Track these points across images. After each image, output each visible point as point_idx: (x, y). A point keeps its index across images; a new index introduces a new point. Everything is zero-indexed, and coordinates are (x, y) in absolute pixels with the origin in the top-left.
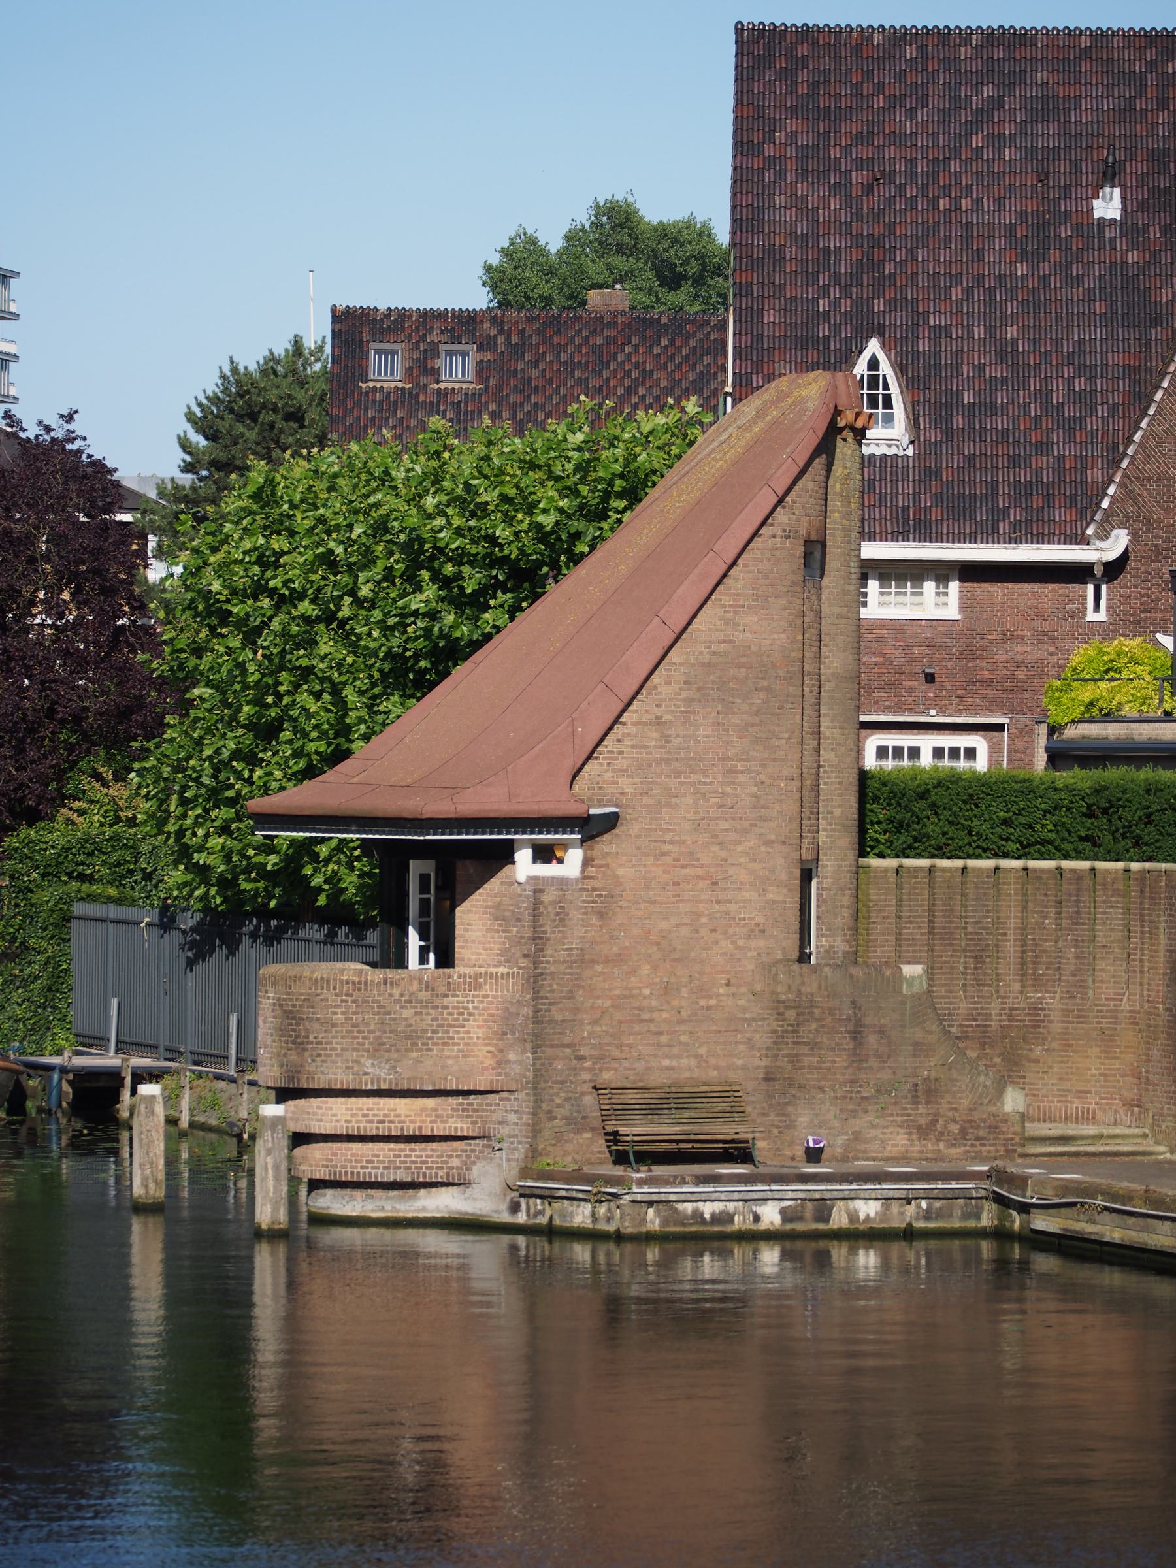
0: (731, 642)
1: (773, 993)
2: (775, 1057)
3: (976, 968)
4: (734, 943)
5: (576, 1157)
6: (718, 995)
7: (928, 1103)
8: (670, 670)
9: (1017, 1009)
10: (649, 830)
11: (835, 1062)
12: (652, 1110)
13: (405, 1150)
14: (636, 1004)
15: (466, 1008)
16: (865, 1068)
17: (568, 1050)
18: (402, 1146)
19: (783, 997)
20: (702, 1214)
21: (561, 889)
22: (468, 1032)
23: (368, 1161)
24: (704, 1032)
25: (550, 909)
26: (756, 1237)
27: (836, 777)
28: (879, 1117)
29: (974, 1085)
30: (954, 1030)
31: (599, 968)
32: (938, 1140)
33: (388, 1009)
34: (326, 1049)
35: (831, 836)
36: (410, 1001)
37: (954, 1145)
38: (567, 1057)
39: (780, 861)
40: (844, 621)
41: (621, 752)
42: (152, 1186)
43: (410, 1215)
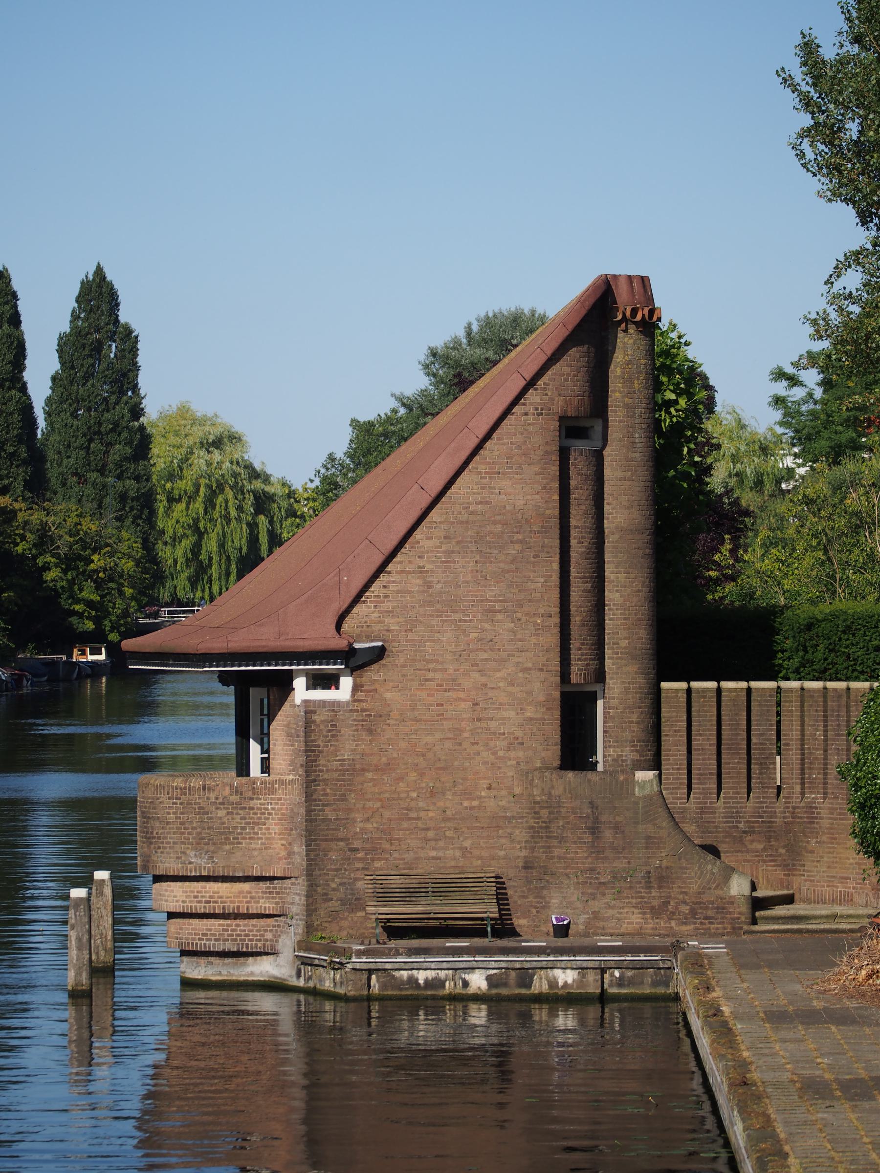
0: (487, 503)
1: (530, 795)
2: (533, 849)
3: (760, 773)
4: (495, 753)
5: (351, 931)
6: (480, 797)
7: (660, 887)
8: (431, 528)
9: (798, 807)
10: (415, 660)
11: (577, 853)
12: (410, 894)
13: (231, 925)
14: (404, 804)
15: (266, 809)
16: (602, 858)
17: (342, 844)
18: (229, 922)
19: (538, 799)
20: (417, 980)
21: (333, 710)
22: (268, 829)
23: (203, 935)
24: (468, 828)
25: (322, 727)
26: (464, 999)
27: (621, 614)
28: (614, 900)
29: (702, 872)
30: (741, 825)
31: (369, 775)
32: (670, 919)
33: (206, 810)
34: (163, 843)
35: (617, 664)
36: (223, 804)
37: (685, 924)
38: (341, 849)
39: (537, 686)
40: (628, 483)
41: (386, 596)
42: (102, 953)
43: (242, 978)
